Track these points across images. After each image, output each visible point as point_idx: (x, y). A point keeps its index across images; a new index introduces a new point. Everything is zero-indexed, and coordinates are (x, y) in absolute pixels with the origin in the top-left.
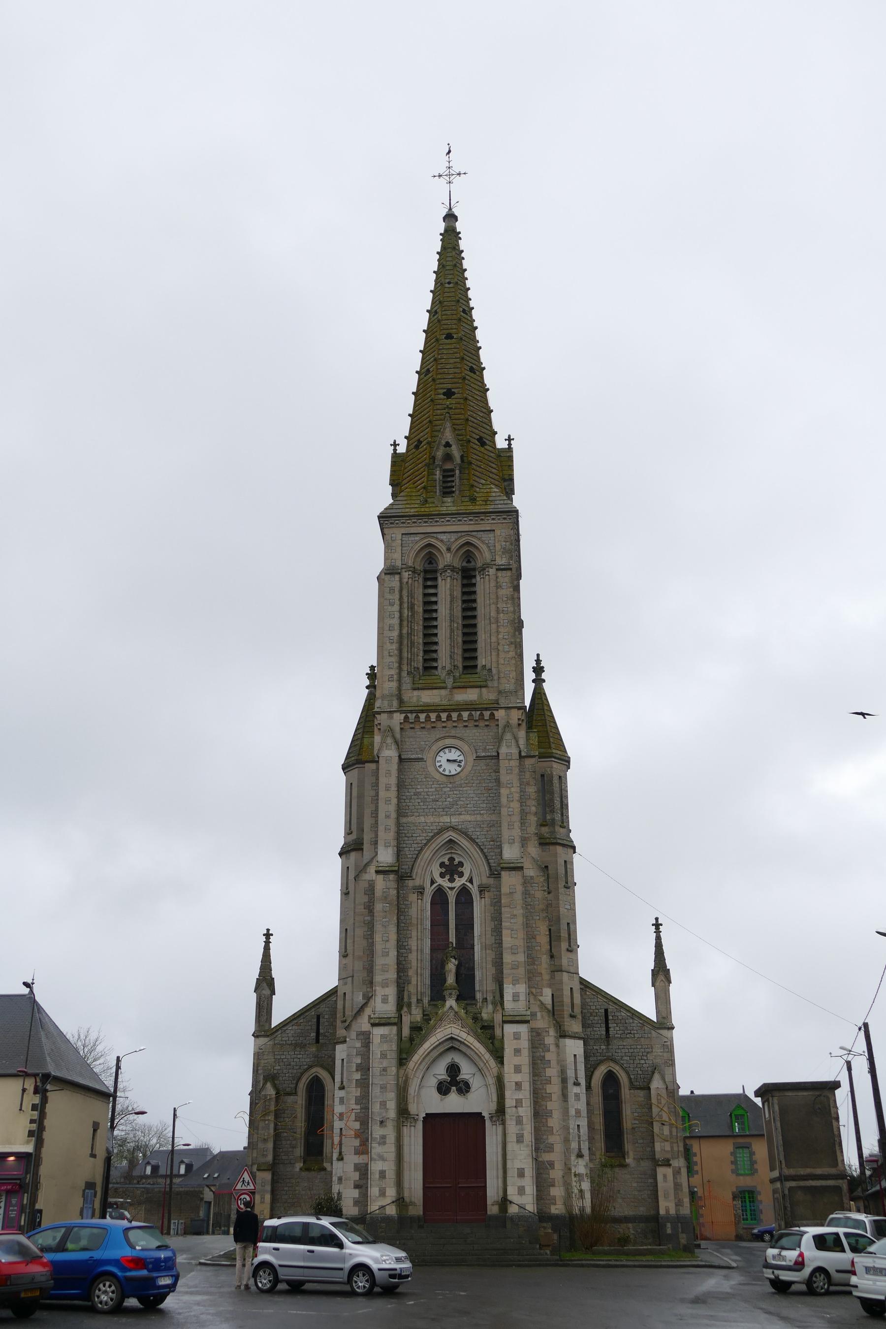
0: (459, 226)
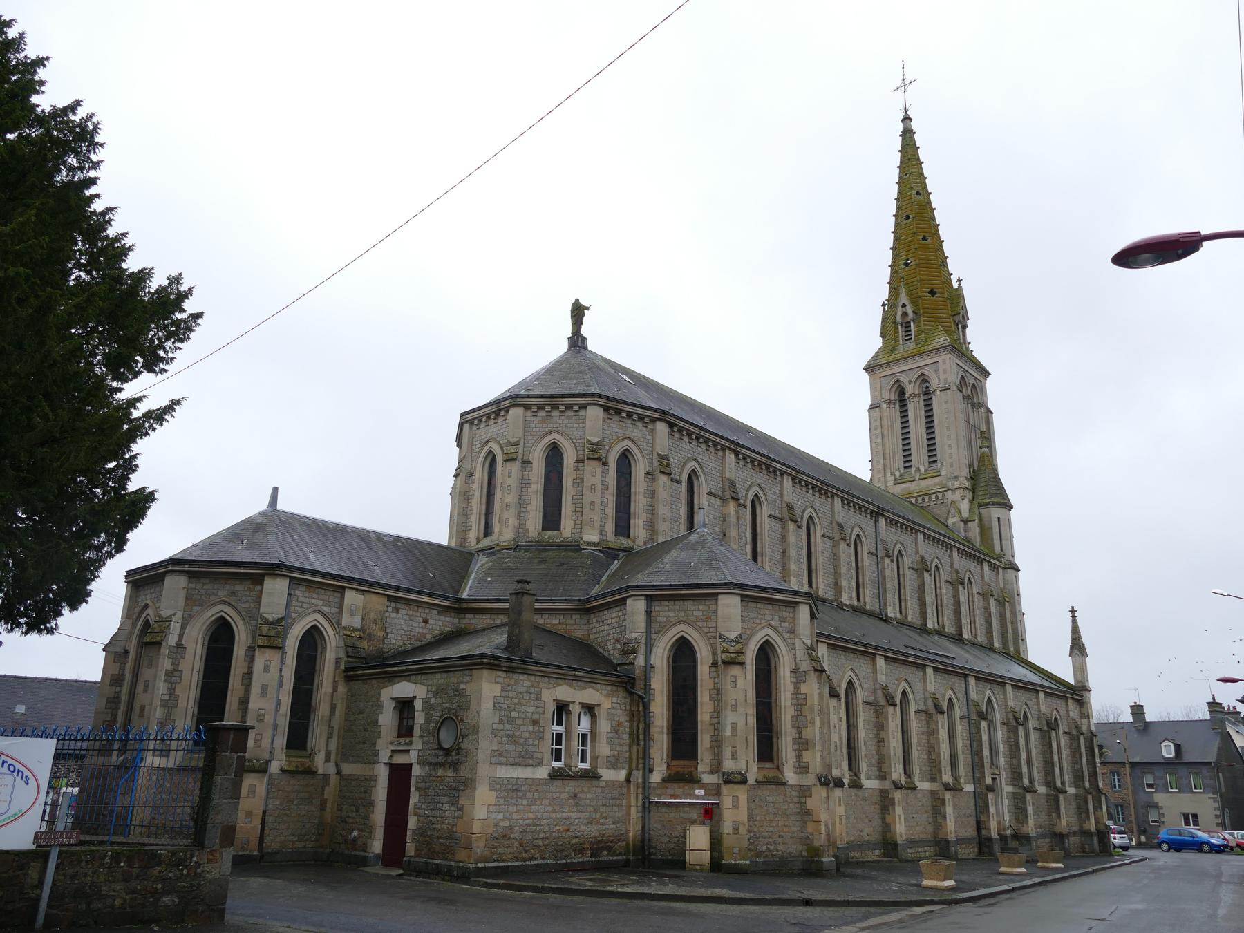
0: (914, 125)
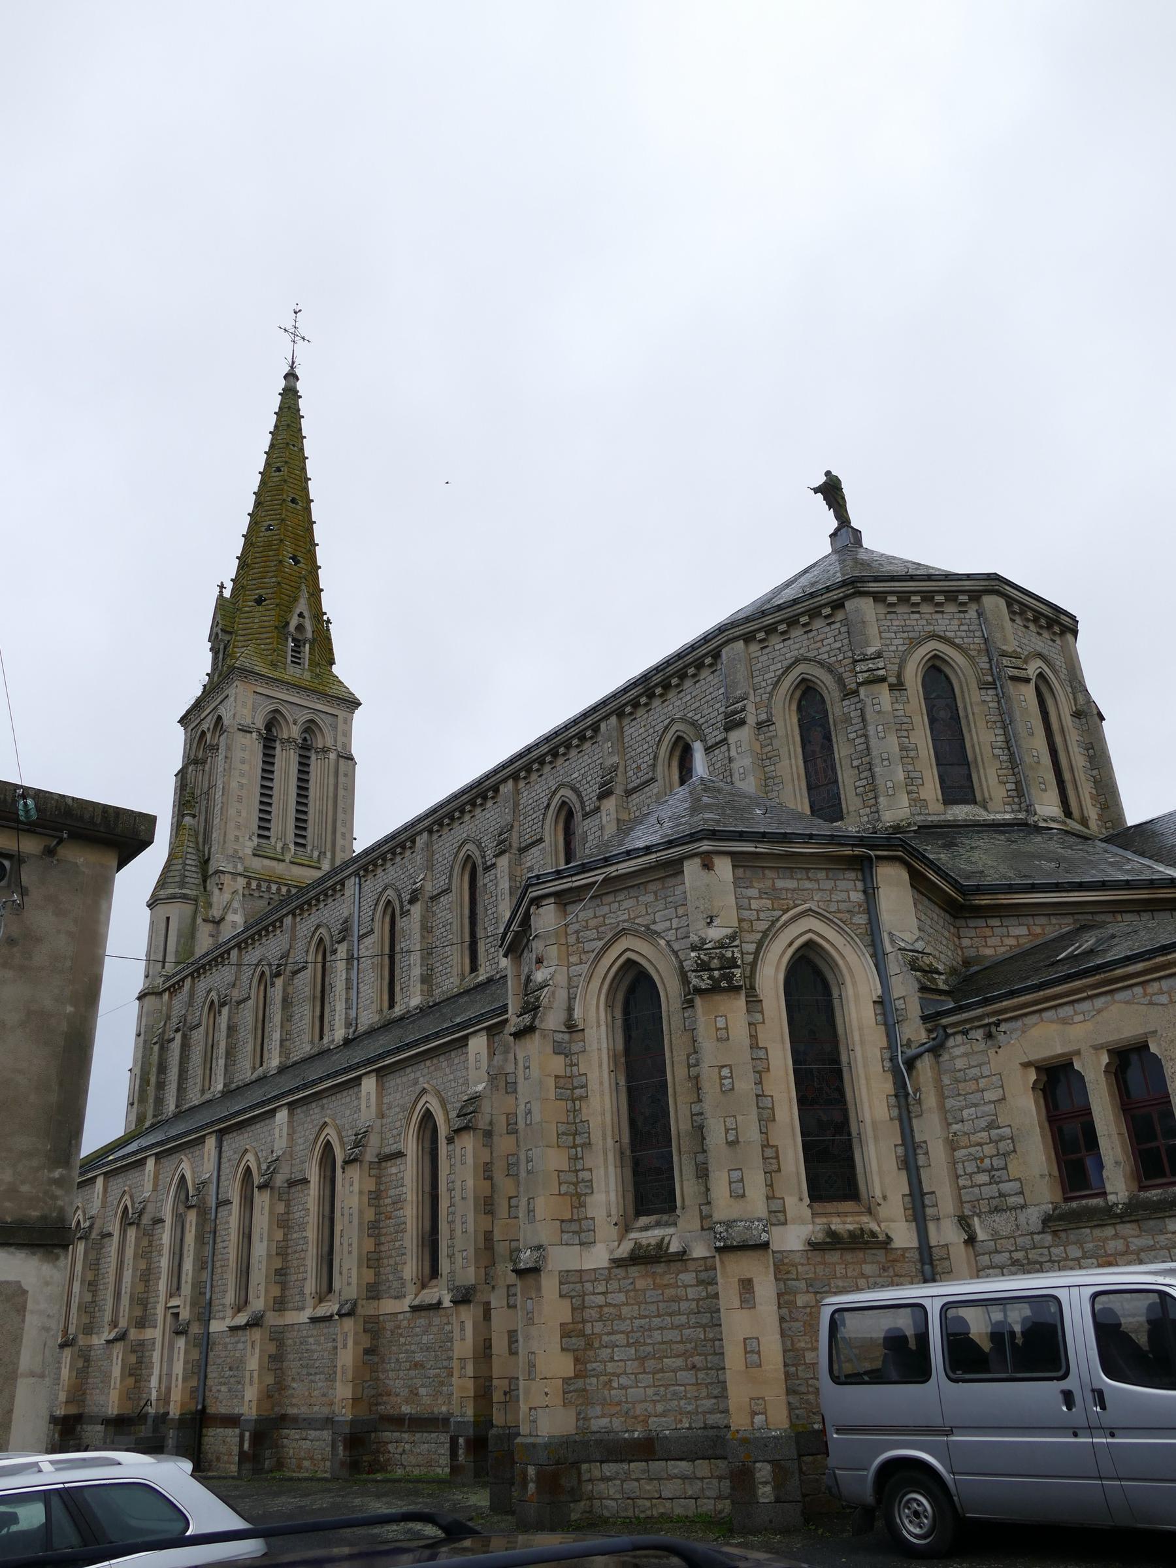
0: (300, 386)
